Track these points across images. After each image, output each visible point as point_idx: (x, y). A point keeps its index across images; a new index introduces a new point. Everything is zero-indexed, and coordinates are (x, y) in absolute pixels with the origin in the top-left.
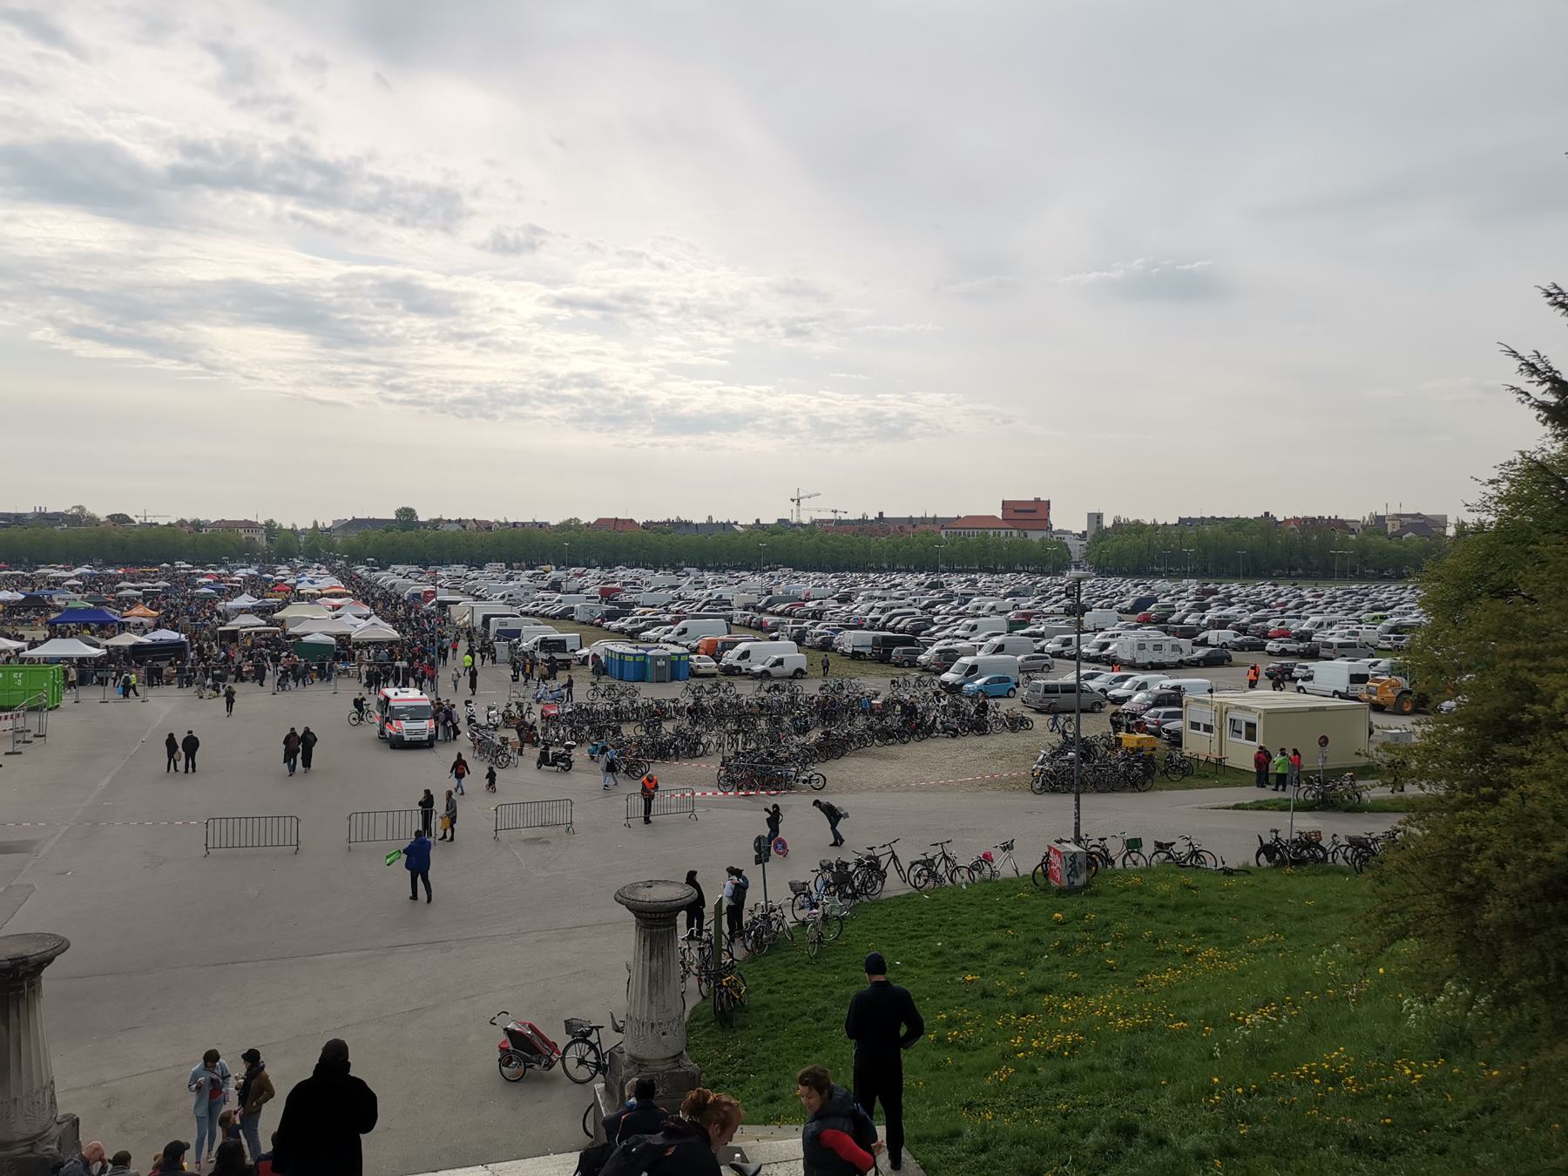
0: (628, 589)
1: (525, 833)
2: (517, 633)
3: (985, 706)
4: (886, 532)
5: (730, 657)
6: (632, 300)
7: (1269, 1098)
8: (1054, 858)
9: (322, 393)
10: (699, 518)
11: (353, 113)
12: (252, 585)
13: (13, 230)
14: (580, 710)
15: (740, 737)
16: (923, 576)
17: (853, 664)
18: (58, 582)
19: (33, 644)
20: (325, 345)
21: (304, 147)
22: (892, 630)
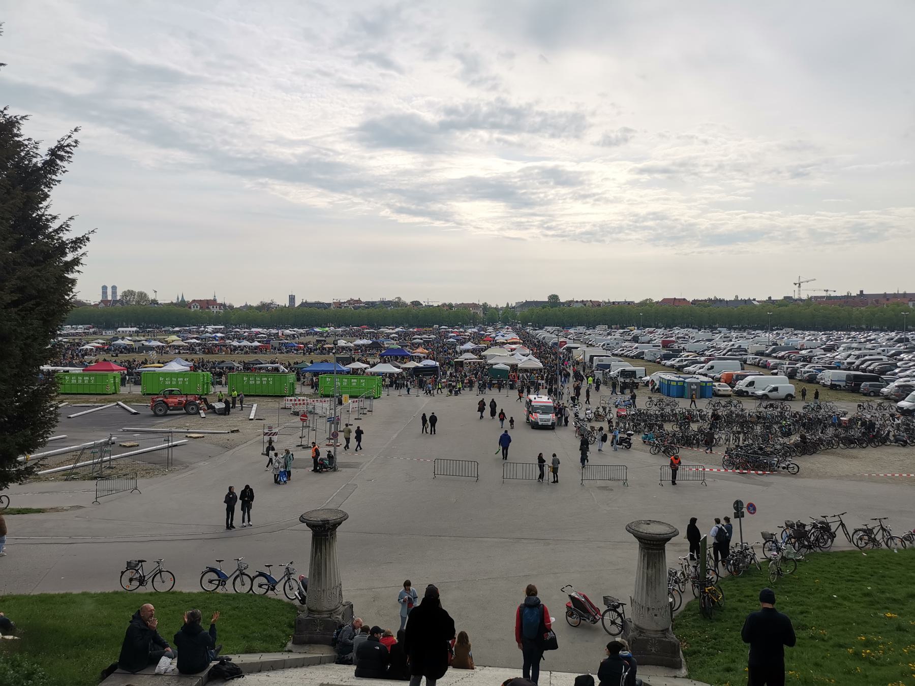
0: (680, 341)
1: (599, 483)
2: (608, 366)
5: (741, 385)
9: (513, 234)
10: (729, 297)
11: (527, 80)
13: (372, 163)
14: (640, 413)
15: (741, 436)
16: (893, 334)
17: (831, 393)
19: (373, 365)
20: (513, 207)
21: (503, 102)
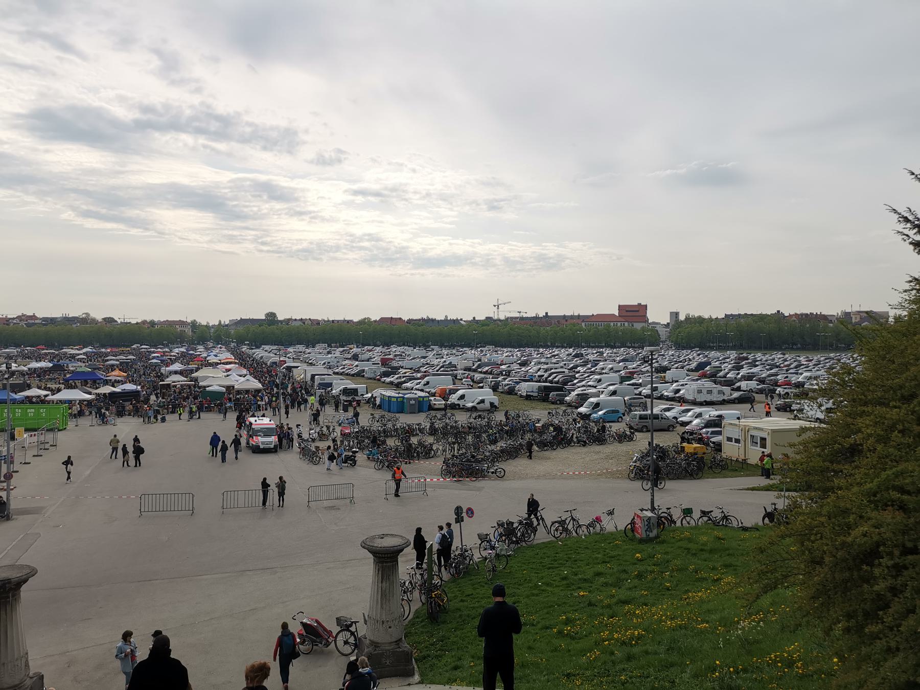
0: (397, 358)
1: (326, 504)
2: (330, 385)
3: (604, 427)
4: (550, 324)
5: (454, 398)
6: (397, 191)
7: (749, 675)
8: (637, 520)
9: (224, 247)
11: (230, 85)
12: (182, 357)
13: (49, 157)
14: (363, 430)
15: (456, 446)
16: (571, 350)
17: (526, 402)
18: (73, 357)
21: (209, 107)
22: (551, 382)
